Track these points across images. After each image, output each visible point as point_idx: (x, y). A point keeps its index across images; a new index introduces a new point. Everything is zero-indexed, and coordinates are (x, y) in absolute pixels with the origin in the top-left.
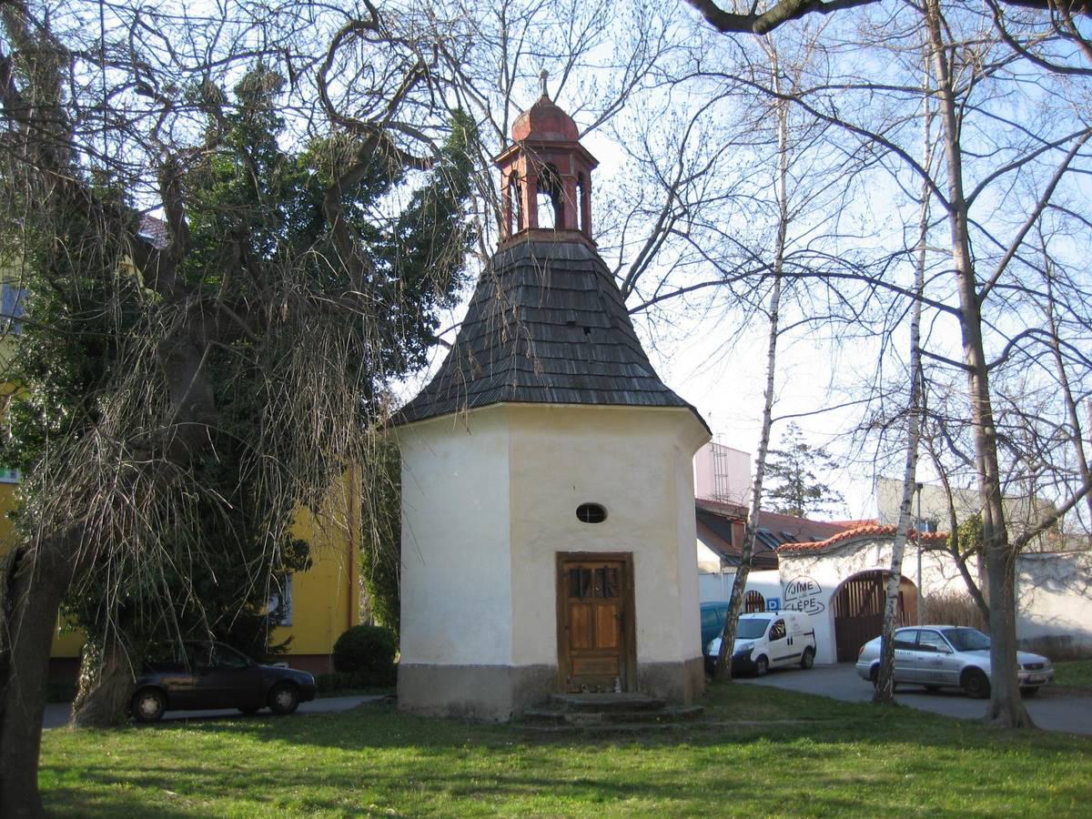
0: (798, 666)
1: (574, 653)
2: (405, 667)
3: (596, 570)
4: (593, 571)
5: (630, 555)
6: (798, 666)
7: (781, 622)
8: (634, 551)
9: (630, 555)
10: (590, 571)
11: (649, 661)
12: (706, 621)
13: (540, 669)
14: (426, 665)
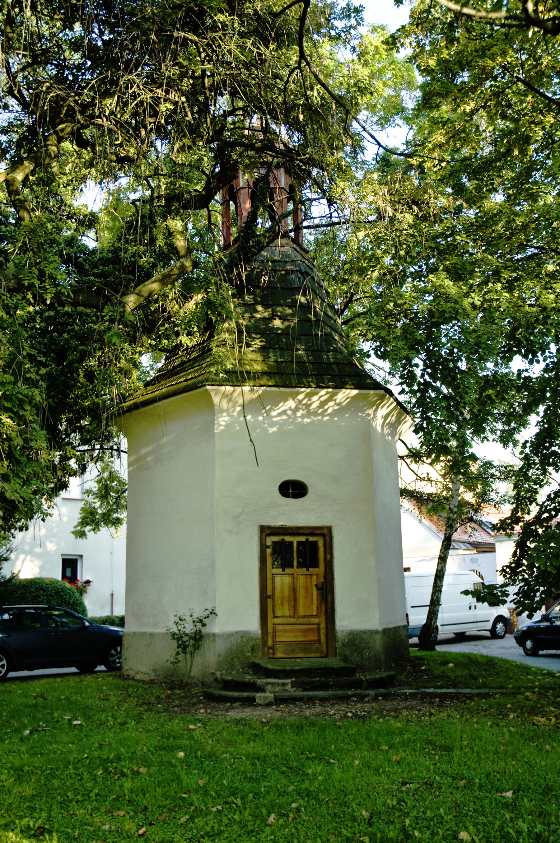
0: (488, 634)
1: (276, 621)
2: (129, 634)
3: (299, 543)
4: (295, 545)
5: (330, 529)
6: (488, 634)
7: (383, 42)
8: (333, 524)
9: (330, 529)
10: (291, 543)
11: (348, 629)
12: (130, 460)
13: (243, 635)
14: (145, 633)
